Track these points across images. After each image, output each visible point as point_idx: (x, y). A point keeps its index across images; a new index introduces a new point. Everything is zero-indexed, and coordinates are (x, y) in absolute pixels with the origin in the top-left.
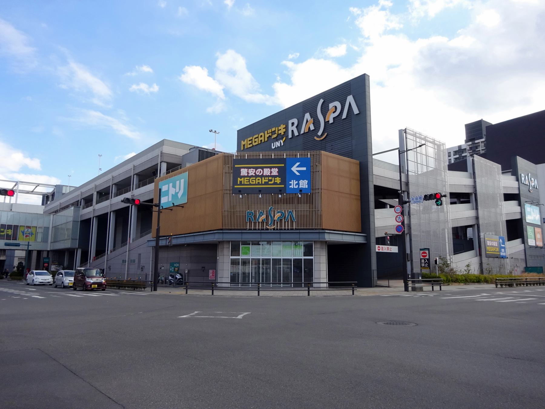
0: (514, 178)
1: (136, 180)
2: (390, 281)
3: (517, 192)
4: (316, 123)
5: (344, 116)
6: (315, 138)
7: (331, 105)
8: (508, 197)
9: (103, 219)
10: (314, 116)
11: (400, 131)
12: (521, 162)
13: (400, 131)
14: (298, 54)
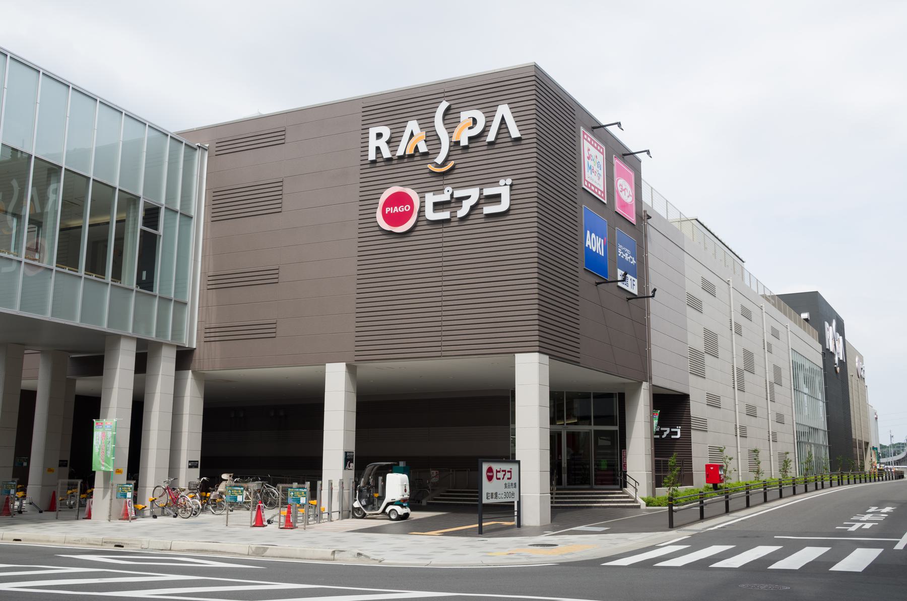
5: (491, 137)
14: (633, 262)
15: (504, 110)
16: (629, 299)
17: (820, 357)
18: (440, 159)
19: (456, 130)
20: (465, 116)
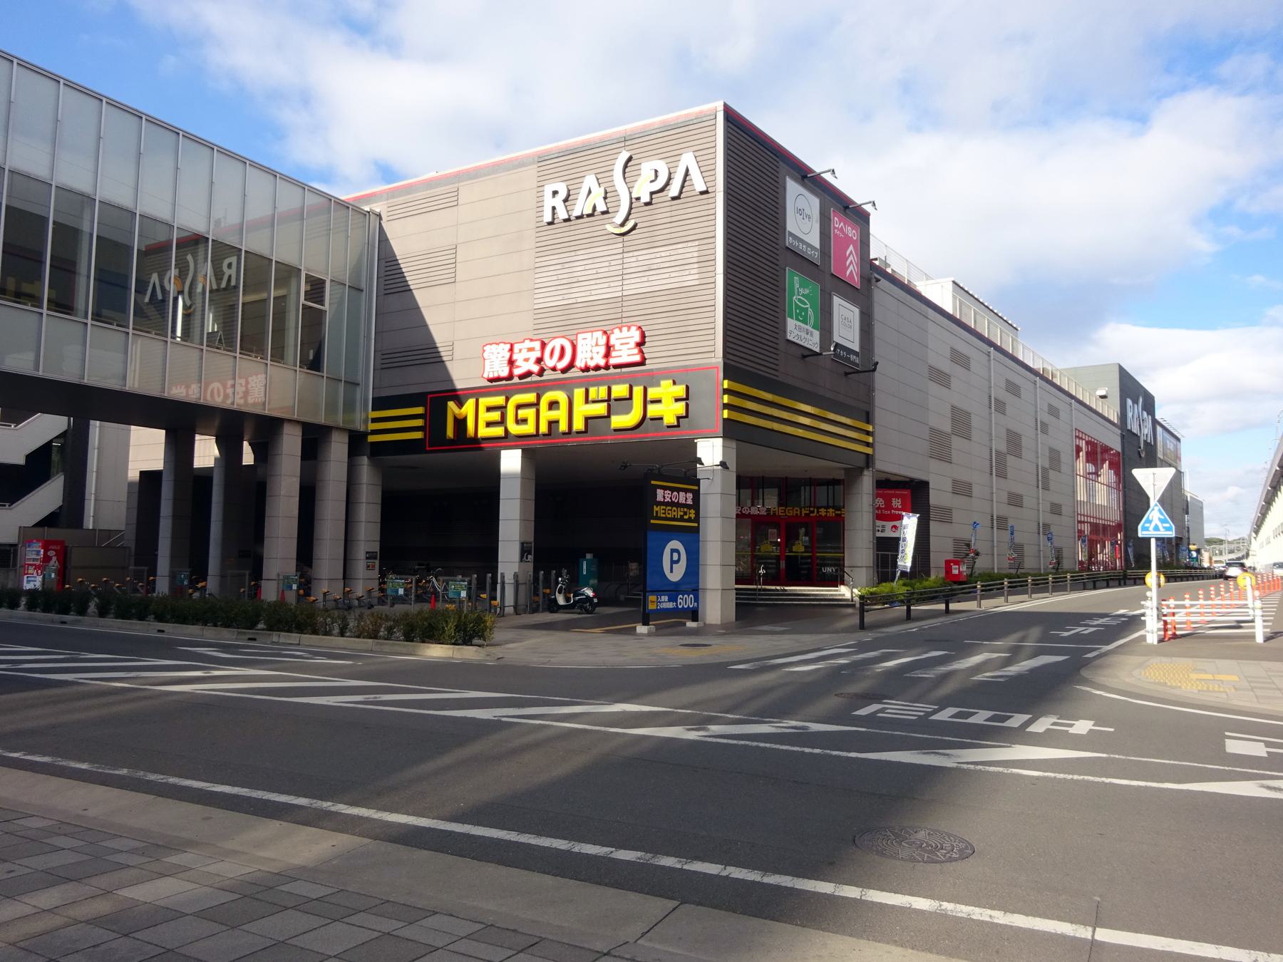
5: (674, 190)
15: (688, 160)
16: (846, 374)
17: (1119, 439)
18: (619, 218)
19: (637, 185)
20: (647, 168)
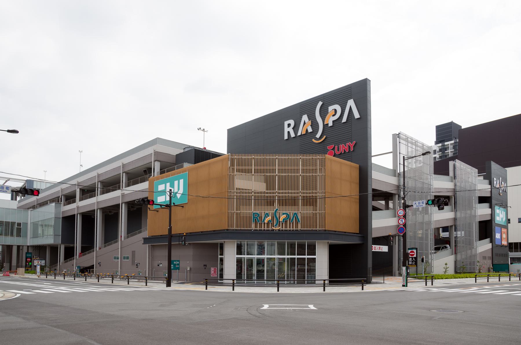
0: (487, 181)
1: (124, 179)
2: (386, 278)
3: (489, 195)
4: (314, 125)
5: (344, 120)
6: (313, 140)
7: (331, 108)
8: (482, 200)
9: (88, 218)
10: (312, 118)
11: (394, 135)
12: (495, 167)
13: (394, 135)
